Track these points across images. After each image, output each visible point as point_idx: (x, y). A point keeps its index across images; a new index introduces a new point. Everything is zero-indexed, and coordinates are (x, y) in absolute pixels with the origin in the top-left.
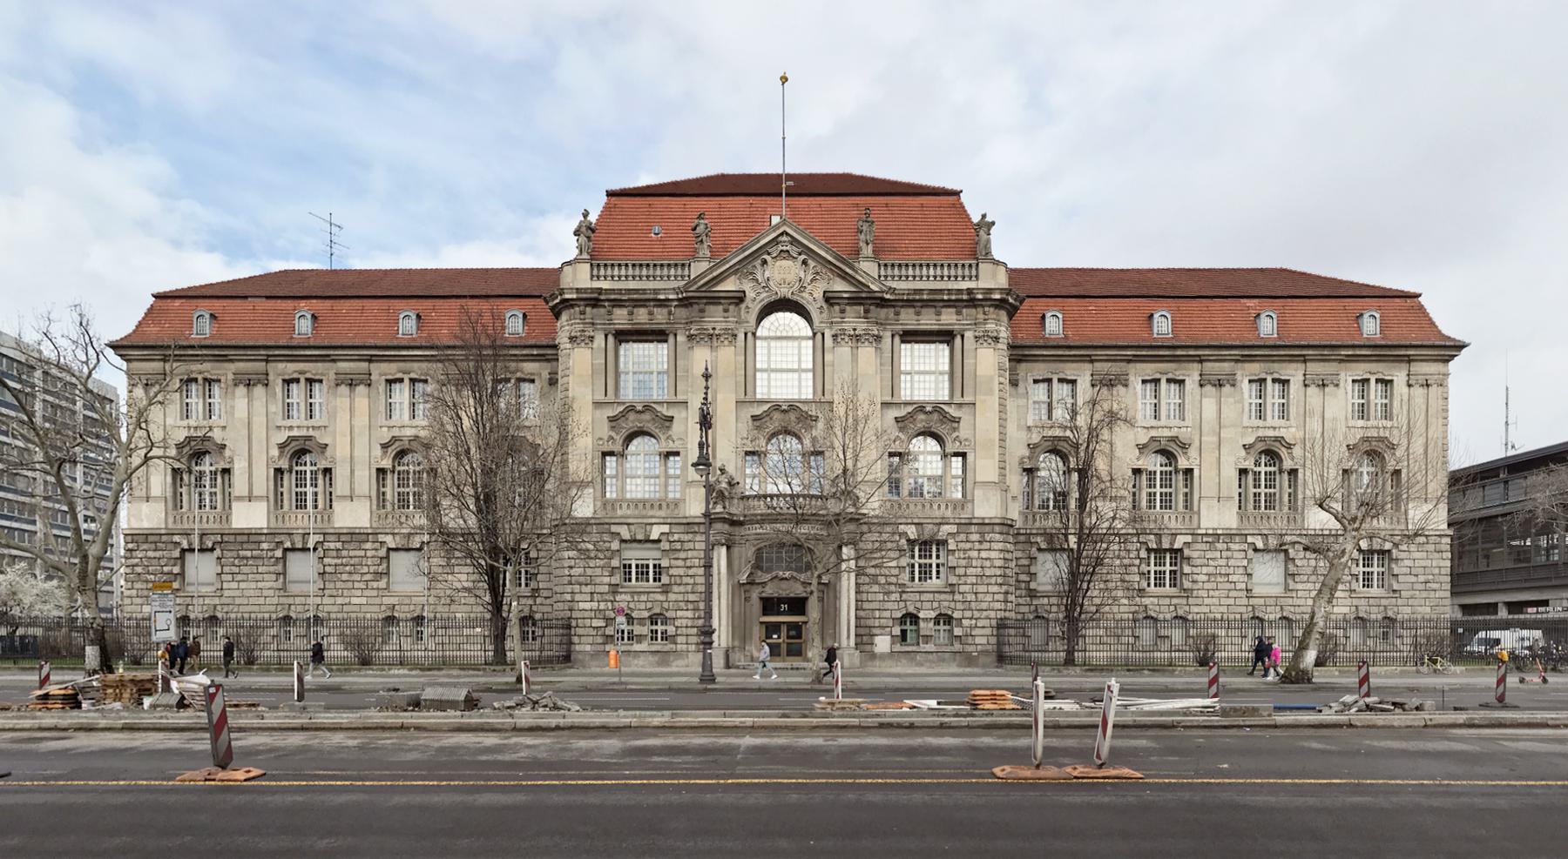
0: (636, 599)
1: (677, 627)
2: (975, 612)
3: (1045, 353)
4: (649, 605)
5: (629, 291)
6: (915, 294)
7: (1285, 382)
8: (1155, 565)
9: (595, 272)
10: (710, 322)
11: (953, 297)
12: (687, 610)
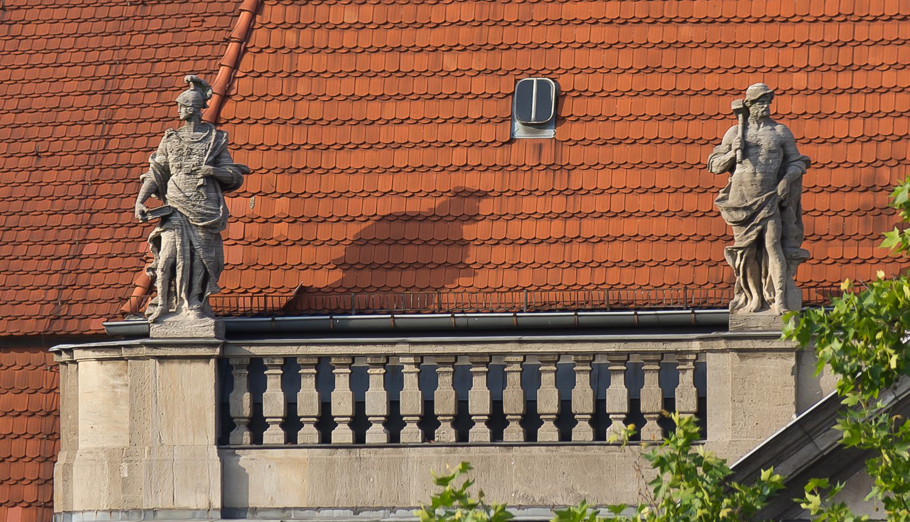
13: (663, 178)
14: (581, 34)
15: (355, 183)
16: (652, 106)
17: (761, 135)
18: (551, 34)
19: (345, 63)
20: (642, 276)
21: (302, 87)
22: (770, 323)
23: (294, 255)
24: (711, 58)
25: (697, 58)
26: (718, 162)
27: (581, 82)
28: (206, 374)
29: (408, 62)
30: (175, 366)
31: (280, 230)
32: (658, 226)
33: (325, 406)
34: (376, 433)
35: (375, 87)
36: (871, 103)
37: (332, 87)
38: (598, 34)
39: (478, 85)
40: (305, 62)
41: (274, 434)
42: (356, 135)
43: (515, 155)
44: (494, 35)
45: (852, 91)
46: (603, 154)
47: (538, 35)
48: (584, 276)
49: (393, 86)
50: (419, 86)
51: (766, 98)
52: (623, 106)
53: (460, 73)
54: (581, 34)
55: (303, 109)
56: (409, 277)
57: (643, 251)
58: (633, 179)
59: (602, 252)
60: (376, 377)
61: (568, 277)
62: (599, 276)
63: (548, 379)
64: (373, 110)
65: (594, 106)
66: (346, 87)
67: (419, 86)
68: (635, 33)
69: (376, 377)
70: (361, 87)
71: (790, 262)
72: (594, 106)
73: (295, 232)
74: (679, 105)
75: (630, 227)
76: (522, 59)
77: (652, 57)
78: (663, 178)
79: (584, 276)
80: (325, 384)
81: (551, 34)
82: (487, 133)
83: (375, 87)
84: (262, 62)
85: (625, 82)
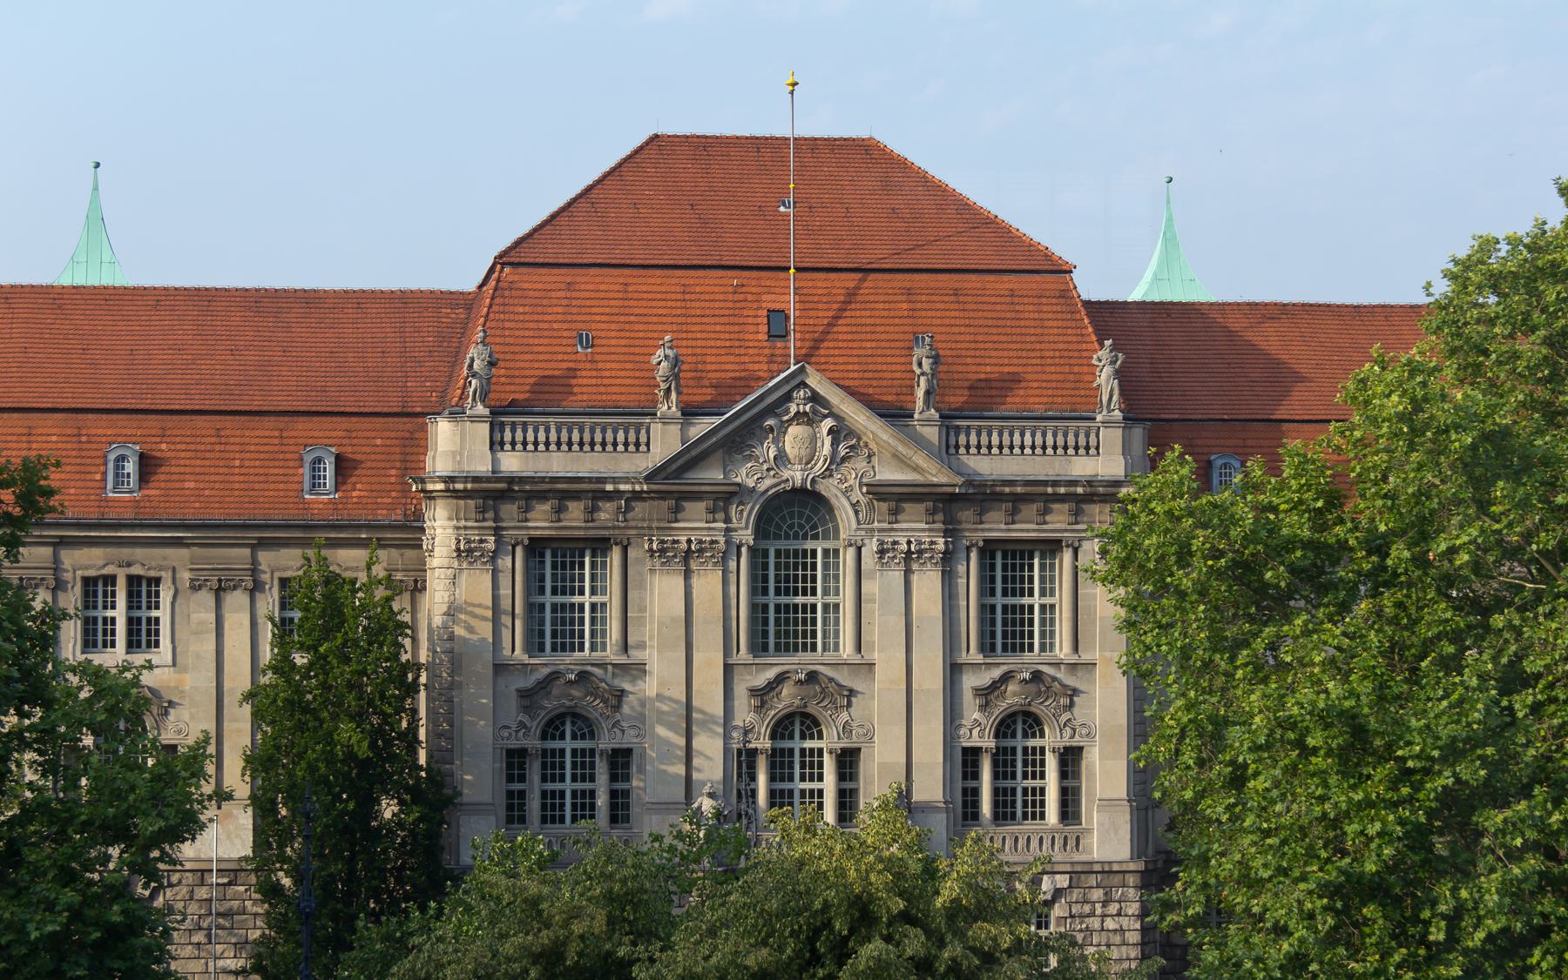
11: (1062, 490)
13: (628, 366)
14: (598, 318)
15: (527, 365)
16: (623, 342)
17: (670, 353)
18: (588, 318)
19: (520, 325)
20: (623, 398)
21: (507, 333)
23: (508, 388)
24: (641, 327)
25: (636, 327)
26: (655, 362)
27: (599, 334)
28: (486, 426)
29: (542, 325)
31: (503, 379)
32: (627, 381)
33: (525, 438)
34: (541, 447)
35: (531, 333)
36: (694, 343)
37: (517, 333)
38: (604, 318)
39: (565, 334)
40: (507, 325)
41: (508, 447)
42: (526, 349)
43: (579, 357)
44: (569, 318)
45: (687, 339)
46: (608, 358)
48: (604, 397)
49: (537, 333)
50: (546, 333)
52: (613, 342)
53: (559, 330)
54: (598, 318)
55: (508, 340)
56: (547, 396)
57: (623, 389)
59: (610, 389)
60: (542, 429)
61: (599, 397)
62: (609, 397)
63: (598, 431)
64: (531, 341)
65: (604, 342)
66: (521, 333)
67: (546, 333)
68: (615, 318)
69: (542, 429)
70: (527, 333)
71: (679, 393)
72: (604, 342)
73: (508, 380)
74: (632, 342)
75: (618, 381)
76: (580, 326)
79: (604, 397)
80: (525, 431)
81: (588, 318)
82: (569, 349)
83: (531, 333)
84: (493, 324)
85: (614, 334)
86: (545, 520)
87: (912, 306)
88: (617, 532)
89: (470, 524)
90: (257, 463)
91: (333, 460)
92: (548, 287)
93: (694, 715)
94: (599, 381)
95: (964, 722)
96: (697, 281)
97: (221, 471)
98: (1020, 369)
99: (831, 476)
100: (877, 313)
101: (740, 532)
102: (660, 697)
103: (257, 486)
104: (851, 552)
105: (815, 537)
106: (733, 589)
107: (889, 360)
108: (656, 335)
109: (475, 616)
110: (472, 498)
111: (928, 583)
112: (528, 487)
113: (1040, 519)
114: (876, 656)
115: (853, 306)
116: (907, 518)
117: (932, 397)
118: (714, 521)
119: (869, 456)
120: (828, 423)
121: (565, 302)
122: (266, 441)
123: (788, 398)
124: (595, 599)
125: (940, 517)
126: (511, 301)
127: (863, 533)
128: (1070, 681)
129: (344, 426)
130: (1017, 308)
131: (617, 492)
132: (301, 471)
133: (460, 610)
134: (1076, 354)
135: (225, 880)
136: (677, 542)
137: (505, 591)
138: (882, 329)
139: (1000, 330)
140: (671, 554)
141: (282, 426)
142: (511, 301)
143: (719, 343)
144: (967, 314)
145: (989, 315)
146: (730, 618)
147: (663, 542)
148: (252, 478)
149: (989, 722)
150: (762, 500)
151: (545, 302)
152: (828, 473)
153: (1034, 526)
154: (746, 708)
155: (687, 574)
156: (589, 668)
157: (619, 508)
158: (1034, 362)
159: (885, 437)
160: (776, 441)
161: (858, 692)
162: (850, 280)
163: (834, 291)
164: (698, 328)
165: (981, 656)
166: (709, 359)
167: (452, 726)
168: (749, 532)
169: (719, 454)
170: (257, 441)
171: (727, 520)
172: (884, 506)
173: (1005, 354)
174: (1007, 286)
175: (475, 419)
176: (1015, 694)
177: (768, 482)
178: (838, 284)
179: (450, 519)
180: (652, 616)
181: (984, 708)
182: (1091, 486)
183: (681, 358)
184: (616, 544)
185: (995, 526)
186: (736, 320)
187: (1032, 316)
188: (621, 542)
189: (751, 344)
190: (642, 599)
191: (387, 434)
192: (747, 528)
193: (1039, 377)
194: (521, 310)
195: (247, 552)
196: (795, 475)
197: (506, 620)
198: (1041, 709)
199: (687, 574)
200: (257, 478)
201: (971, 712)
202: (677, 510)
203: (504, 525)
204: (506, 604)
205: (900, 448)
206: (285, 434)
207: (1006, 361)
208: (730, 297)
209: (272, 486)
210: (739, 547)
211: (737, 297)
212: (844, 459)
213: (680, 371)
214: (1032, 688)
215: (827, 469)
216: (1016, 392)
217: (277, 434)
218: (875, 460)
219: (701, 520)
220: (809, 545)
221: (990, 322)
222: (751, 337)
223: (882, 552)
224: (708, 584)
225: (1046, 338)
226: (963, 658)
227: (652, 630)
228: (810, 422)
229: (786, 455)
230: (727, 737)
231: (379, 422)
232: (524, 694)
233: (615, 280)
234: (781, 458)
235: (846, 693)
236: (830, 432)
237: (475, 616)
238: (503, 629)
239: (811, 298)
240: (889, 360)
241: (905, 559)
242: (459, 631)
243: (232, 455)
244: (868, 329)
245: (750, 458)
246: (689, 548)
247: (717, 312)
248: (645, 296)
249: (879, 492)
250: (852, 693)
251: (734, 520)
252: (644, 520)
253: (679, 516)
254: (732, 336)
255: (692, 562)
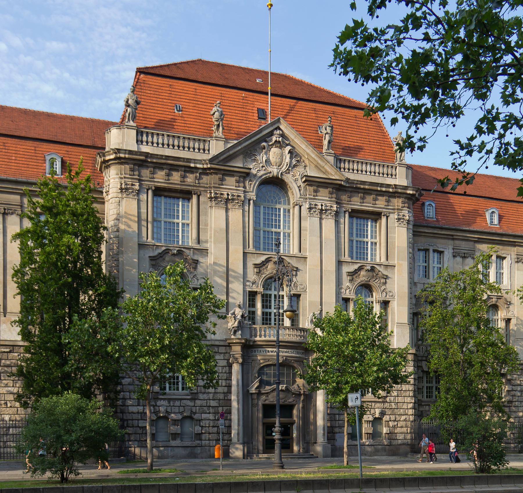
0: (172, 404)
1: (202, 427)
2: (397, 416)
3: (426, 231)
4: (182, 409)
5: (168, 157)
6: (361, 184)
7: (441, 253)
8: (427, 383)
9: (140, 138)
10: (226, 189)
11: (384, 189)
12: (209, 413)
13: (198, 121)
19: (149, 98)
22: (38, 271)
23: (144, 122)
24: (203, 107)
26: (212, 113)
28: (135, 131)
30: (130, 130)
31: (141, 118)
40: (143, 97)
41: (145, 143)
43: (176, 115)
47: (178, 99)
49: (156, 102)
51: (220, 103)
52: (191, 111)
58: (194, 120)
59: (190, 129)
66: (149, 101)
67: (160, 103)
70: (152, 102)
73: (144, 119)
77: (194, 105)
78: (198, 121)
83: (154, 102)
85: (191, 108)
86: (163, 179)
87: (316, 115)
88: (195, 188)
89: (127, 176)
90: (23, 159)
91: (60, 160)
92: (161, 85)
93: (230, 273)
94: (185, 125)
95: (343, 287)
96: (227, 93)
97: (5, 160)
98: (361, 145)
99: (289, 173)
100: (302, 116)
101: (250, 194)
102: (215, 263)
103: (23, 169)
104: (297, 208)
105: (280, 203)
106: (247, 219)
107: (309, 134)
108: (215, 99)
109: (131, 220)
110: (127, 163)
111: (329, 224)
112: (155, 161)
113: (374, 202)
114: (308, 254)
115: (293, 112)
116: (321, 195)
117: (330, 145)
118: (239, 187)
119: (305, 166)
120: (289, 148)
121: (169, 92)
122: (28, 151)
123: (271, 134)
124: (184, 221)
125: (334, 196)
126: (144, 88)
127: (302, 200)
128: (385, 273)
129: (65, 149)
130: (358, 122)
131: (196, 168)
132: (44, 165)
133: (122, 217)
134: (382, 142)
135: (8, 350)
136: (222, 194)
137: (143, 210)
138: (305, 122)
139: (352, 129)
140: (220, 200)
141: (36, 145)
142: (144, 88)
143: (237, 118)
144: (339, 122)
145: (347, 123)
146: (246, 232)
147: (216, 194)
148: (21, 165)
149: (353, 287)
150: (259, 180)
151: (160, 91)
152: (288, 171)
153: (371, 205)
154: (252, 273)
155: (227, 210)
156: (183, 249)
157: (196, 177)
158: (367, 142)
159: (313, 156)
160: (266, 153)
161: (300, 270)
162: (292, 102)
163: (284, 105)
164: (228, 110)
165: (350, 259)
166: (233, 123)
167: (118, 272)
168: (254, 194)
169: (241, 157)
170: (23, 150)
171: (245, 187)
172: (312, 188)
173: (355, 138)
174: (353, 113)
175: (129, 127)
176: (364, 276)
177: (262, 173)
178: (286, 103)
179: (117, 174)
180: (211, 228)
181: (351, 281)
182: (396, 188)
183: (224, 113)
184: (194, 194)
185: (356, 203)
186: (244, 110)
187: (364, 126)
188: (197, 193)
189: (251, 120)
190: (206, 220)
191: (86, 155)
192: (253, 192)
193: (369, 148)
194: (149, 92)
195: (18, 197)
196: (274, 171)
197: (144, 223)
198: (374, 284)
199: (227, 210)
200: (23, 165)
201: (346, 282)
202: (222, 180)
203: (143, 179)
204: (144, 216)
205: (320, 162)
206: (37, 149)
207: (356, 141)
208: (241, 101)
209: (30, 170)
210: (249, 200)
211: (244, 101)
212: (295, 166)
213: (224, 117)
214: (370, 274)
215: (287, 169)
216: (361, 153)
217: (33, 148)
218: (308, 168)
219: (233, 186)
220: (278, 206)
221: (348, 126)
222: (251, 117)
223: (310, 209)
224: (236, 215)
225: (370, 135)
226: (343, 259)
227: (211, 234)
228: (281, 147)
229: (270, 161)
230: (244, 285)
231: (81, 149)
232: (152, 259)
233: (191, 87)
234: (268, 161)
235: (295, 269)
236: (290, 152)
237: (131, 220)
238: (143, 227)
239: (275, 106)
240: (309, 134)
241: (320, 212)
242: (122, 227)
243: (11, 155)
244: (299, 121)
245: (255, 160)
246: (228, 197)
247: (236, 106)
248: (204, 95)
249: (309, 181)
250: (297, 270)
251: (247, 188)
252: (207, 184)
253: (223, 183)
254: (243, 116)
255: (229, 204)
